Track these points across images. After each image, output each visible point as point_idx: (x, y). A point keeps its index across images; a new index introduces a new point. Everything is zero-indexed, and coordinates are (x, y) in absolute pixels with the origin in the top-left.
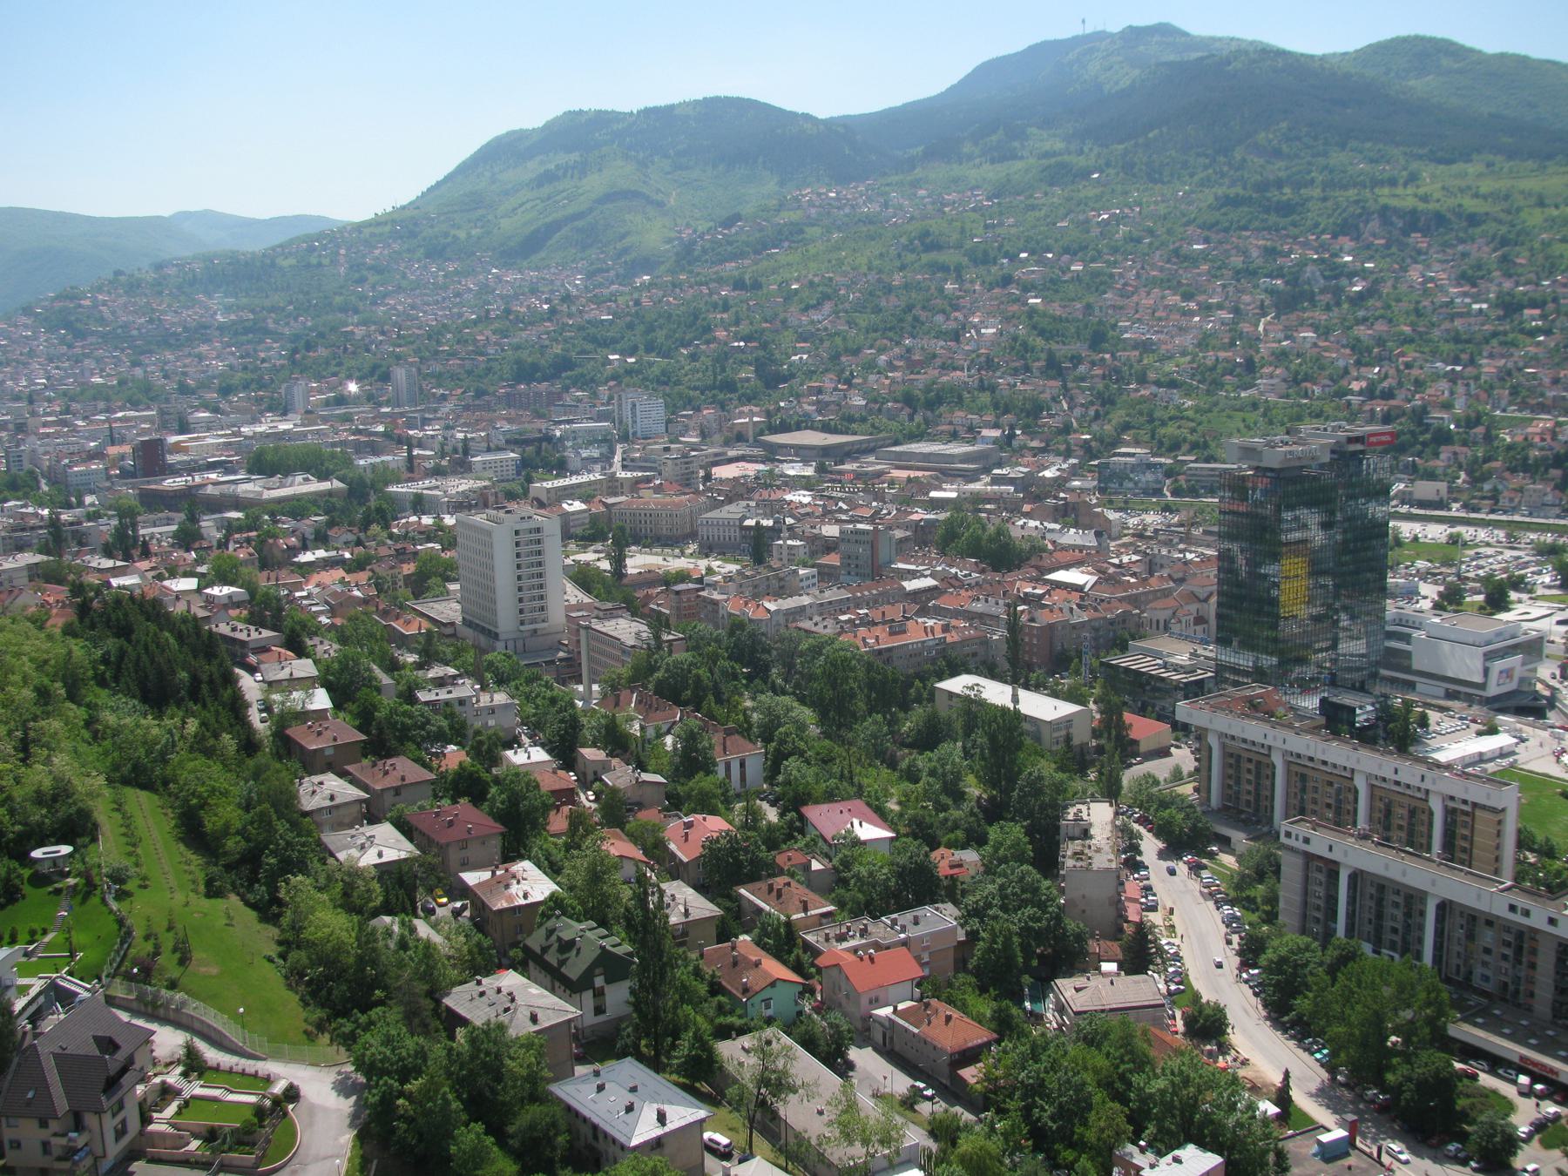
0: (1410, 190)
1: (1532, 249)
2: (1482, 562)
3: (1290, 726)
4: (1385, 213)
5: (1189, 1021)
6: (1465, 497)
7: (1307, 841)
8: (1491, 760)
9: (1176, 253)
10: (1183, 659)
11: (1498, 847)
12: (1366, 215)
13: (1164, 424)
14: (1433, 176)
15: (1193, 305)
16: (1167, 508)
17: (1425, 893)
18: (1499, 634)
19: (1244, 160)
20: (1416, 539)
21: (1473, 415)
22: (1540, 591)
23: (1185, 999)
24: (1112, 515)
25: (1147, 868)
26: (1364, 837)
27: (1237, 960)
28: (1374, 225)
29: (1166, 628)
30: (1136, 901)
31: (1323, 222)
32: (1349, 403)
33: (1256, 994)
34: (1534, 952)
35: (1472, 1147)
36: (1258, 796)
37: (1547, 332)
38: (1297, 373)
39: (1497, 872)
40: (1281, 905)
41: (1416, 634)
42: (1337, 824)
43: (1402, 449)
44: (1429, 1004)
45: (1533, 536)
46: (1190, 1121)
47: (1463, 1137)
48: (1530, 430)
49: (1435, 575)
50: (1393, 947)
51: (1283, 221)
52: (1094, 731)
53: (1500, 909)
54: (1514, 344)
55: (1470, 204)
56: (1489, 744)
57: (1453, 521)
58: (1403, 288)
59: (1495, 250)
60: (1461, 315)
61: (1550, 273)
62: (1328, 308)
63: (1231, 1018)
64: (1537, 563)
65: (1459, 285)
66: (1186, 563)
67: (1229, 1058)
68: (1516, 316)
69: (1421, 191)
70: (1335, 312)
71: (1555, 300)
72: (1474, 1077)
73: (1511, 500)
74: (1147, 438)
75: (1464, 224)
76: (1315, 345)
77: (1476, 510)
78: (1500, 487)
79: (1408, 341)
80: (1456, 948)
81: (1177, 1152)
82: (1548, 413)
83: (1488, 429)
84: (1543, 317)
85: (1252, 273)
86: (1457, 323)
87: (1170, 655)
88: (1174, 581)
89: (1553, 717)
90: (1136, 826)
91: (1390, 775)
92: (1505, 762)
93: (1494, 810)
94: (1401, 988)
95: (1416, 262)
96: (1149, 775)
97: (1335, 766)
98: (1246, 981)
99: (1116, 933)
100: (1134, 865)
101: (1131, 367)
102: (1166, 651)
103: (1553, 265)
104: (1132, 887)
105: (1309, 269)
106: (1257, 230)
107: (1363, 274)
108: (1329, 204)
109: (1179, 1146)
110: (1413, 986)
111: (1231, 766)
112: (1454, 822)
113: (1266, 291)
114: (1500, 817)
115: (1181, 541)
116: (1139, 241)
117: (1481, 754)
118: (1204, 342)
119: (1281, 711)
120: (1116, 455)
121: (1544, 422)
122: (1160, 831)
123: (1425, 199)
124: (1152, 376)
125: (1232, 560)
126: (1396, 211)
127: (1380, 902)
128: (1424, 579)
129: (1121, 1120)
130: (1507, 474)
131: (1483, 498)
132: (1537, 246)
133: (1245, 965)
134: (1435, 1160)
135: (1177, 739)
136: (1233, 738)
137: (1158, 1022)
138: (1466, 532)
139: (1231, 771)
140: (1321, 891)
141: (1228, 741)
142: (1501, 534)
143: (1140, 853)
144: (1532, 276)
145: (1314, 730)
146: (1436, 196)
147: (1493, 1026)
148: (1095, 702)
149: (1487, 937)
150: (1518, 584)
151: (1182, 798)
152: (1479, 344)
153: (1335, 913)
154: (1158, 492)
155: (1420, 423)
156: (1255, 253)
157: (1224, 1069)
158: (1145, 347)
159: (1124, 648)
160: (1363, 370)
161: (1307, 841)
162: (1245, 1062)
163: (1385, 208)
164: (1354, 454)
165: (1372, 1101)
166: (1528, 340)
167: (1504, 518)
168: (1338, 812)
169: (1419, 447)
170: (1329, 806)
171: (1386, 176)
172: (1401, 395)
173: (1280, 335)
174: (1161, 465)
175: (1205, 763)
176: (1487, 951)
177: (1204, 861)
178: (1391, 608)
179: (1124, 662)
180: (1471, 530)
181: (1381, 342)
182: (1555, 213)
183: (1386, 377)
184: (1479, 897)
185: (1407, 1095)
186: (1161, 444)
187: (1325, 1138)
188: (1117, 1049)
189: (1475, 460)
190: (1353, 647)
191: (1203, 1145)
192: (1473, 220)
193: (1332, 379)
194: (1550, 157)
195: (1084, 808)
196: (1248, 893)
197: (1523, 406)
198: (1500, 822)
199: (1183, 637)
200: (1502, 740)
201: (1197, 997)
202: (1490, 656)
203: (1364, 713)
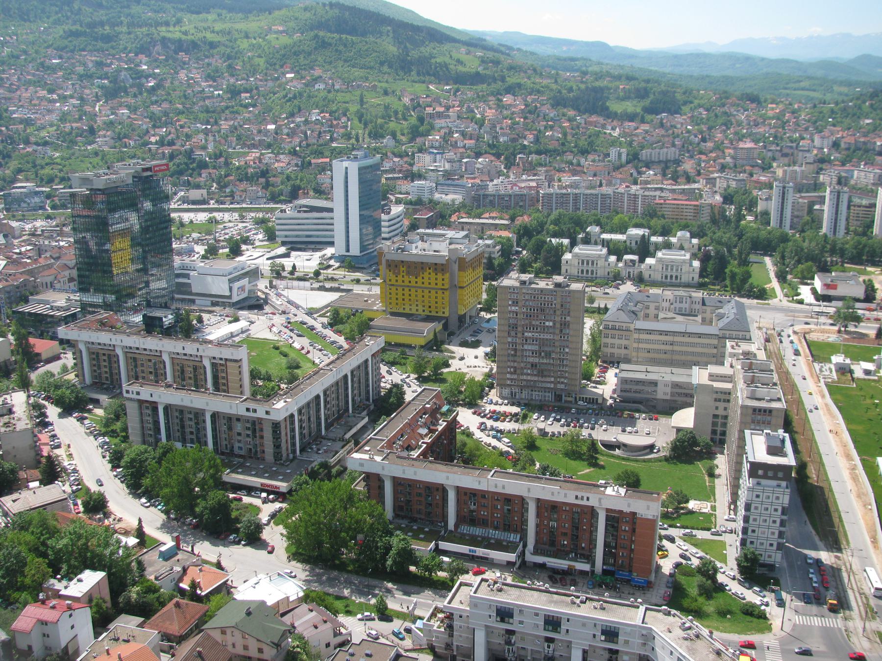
0: (177, 28)
1: (243, 61)
2: (227, 231)
3: (124, 332)
4: (164, 41)
5: (86, 505)
6: (217, 197)
7: (138, 393)
8: (237, 335)
9: (42, 64)
10: (62, 303)
11: (240, 380)
12: (153, 42)
13: (42, 168)
14: (190, 21)
15: (55, 96)
16: (49, 217)
17: (204, 410)
18: (235, 268)
19: (80, 9)
20: (191, 222)
21: (218, 152)
22: (257, 243)
23: (83, 491)
24: (14, 224)
25: (52, 424)
26: (169, 386)
27: (110, 465)
28: (159, 48)
29: (52, 286)
30: (47, 444)
31: (129, 46)
32: (150, 149)
33: (122, 482)
34: (261, 430)
35: (241, 535)
36: (111, 374)
37: (254, 106)
38: (120, 134)
39: (242, 393)
40: (130, 431)
41: (192, 273)
42: (157, 382)
43: (181, 173)
44: (210, 467)
45: (253, 215)
46: (86, 558)
47: (237, 531)
48: (248, 158)
49: (202, 240)
50: (192, 442)
51: (105, 46)
52: (12, 351)
53: (242, 412)
54: (237, 112)
55: (210, 36)
56: (235, 327)
57: (211, 210)
58: (176, 83)
59: (225, 62)
60: (208, 98)
61: (253, 75)
62: (135, 96)
63: (108, 497)
64: (255, 229)
65: (207, 81)
66: (60, 248)
67: (111, 520)
68: (238, 97)
69: (183, 29)
70: (139, 98)
71: (257, 88)
72: (240, 500)
73: (241, 196)
74: (33, 177)
75: (208, 47)
76: (129, 117)
77: (223, 203)
78: (235, 190)
79: (181, 113)
80: (224, 436)
81: (79, 576)
82: (257, 148)
83: (226, 159)
84: (252, 97)
85: (90, 77)
86: (207, 102)
87: (54, 301)
88: (54, 259)
89: (267, 309)
90: (44, 402)
91: (181, 351)
92: (244, 335)
93: (236, 361)
94: (195, 462)
95: (183, 69)
96: (48, 372)
97: (151, 350)
98: (116, 476)
99: (37, 464)
100: (44, 424)
101: (20, 134)
102: (51, 299)
103: (255, 70)
104: (44, 437)
105: (123, 73)
106: (90, 51)
107: (154, 76)
108: (132, 36)
109: (81, 572)
110: (202, 461)
111: (94, 359)
112: (217, 370)
113: (99, 87)
114: (239, 364)
115: (58, 235)
116: (18, 57)
117: (232, 333)
118: (63, 118)
119: (119, 325)
120: (14, 188)
121: (255, 154)
122: (58, 402)
123: (185, 33)
124: (33, 139)
125: (86, 243)
126: (169, 39)
127: (182, 420)
128: (197, 243)
129: (44, 567)
130: (238, 183)
131: (226, 196)
132: (246, 59)
133: (114, 468)
134: (224, 546)
135: (64, 349)
136: (93, 343)
137: (66, 509)
138: (218, 216)
139: (94, 362)
140: (150, 419)
141: (90, 346)
142: (236, 215)
143: (47, 417)
144: (245, 76)
145: (138, 333)
146: (192, 31)
147: (247, 471)
148: (12, 335)
149: (238, 427)
150: (246, 241)
151: (68, 382)
152: (219, 113)
153: (159, 429)
154: (42, 208)
155: (190, 158)
156: (90, 65)
157: (109, 526)
158: (27, 122)
159: (27, 301)
160: (157, 130)
161: (138, 393)
162: (120, 520)
163: (164, 38)
164: (147, 177)
165: (190, 524)
166: (245, 110)
167: (238, 206)
168: (156, 375)
169: (190, 171)
170: (151, 373)
171: (164, 19)
172: (179, 143)
173: (109, 112)
174: (43, 192)
175: (79, 360)
176: (239, 434)
177: (86, 415)
178: (177, 261)
179: (27, 309)
180: (221, 214)
181: (166, 114)
182: (254, 42)
183: (170, 133)
184: (231, 407)
185: (206, 516)
186: (42, 180)
187: (163, 548)
188: (38, 528)
189: (221, 176)
190: (158, 285)
191: (94, 568)
192: (212, 45)
193: (139, 136)
194: (250, 12)
195: (8, 397)
196: (112, 428)
197: (244, 145)
198: (240, 367)
199: (61, 290)
200: (242, 324)
201: (88, 490)
202: (231, 281)
203: (168, 319)
